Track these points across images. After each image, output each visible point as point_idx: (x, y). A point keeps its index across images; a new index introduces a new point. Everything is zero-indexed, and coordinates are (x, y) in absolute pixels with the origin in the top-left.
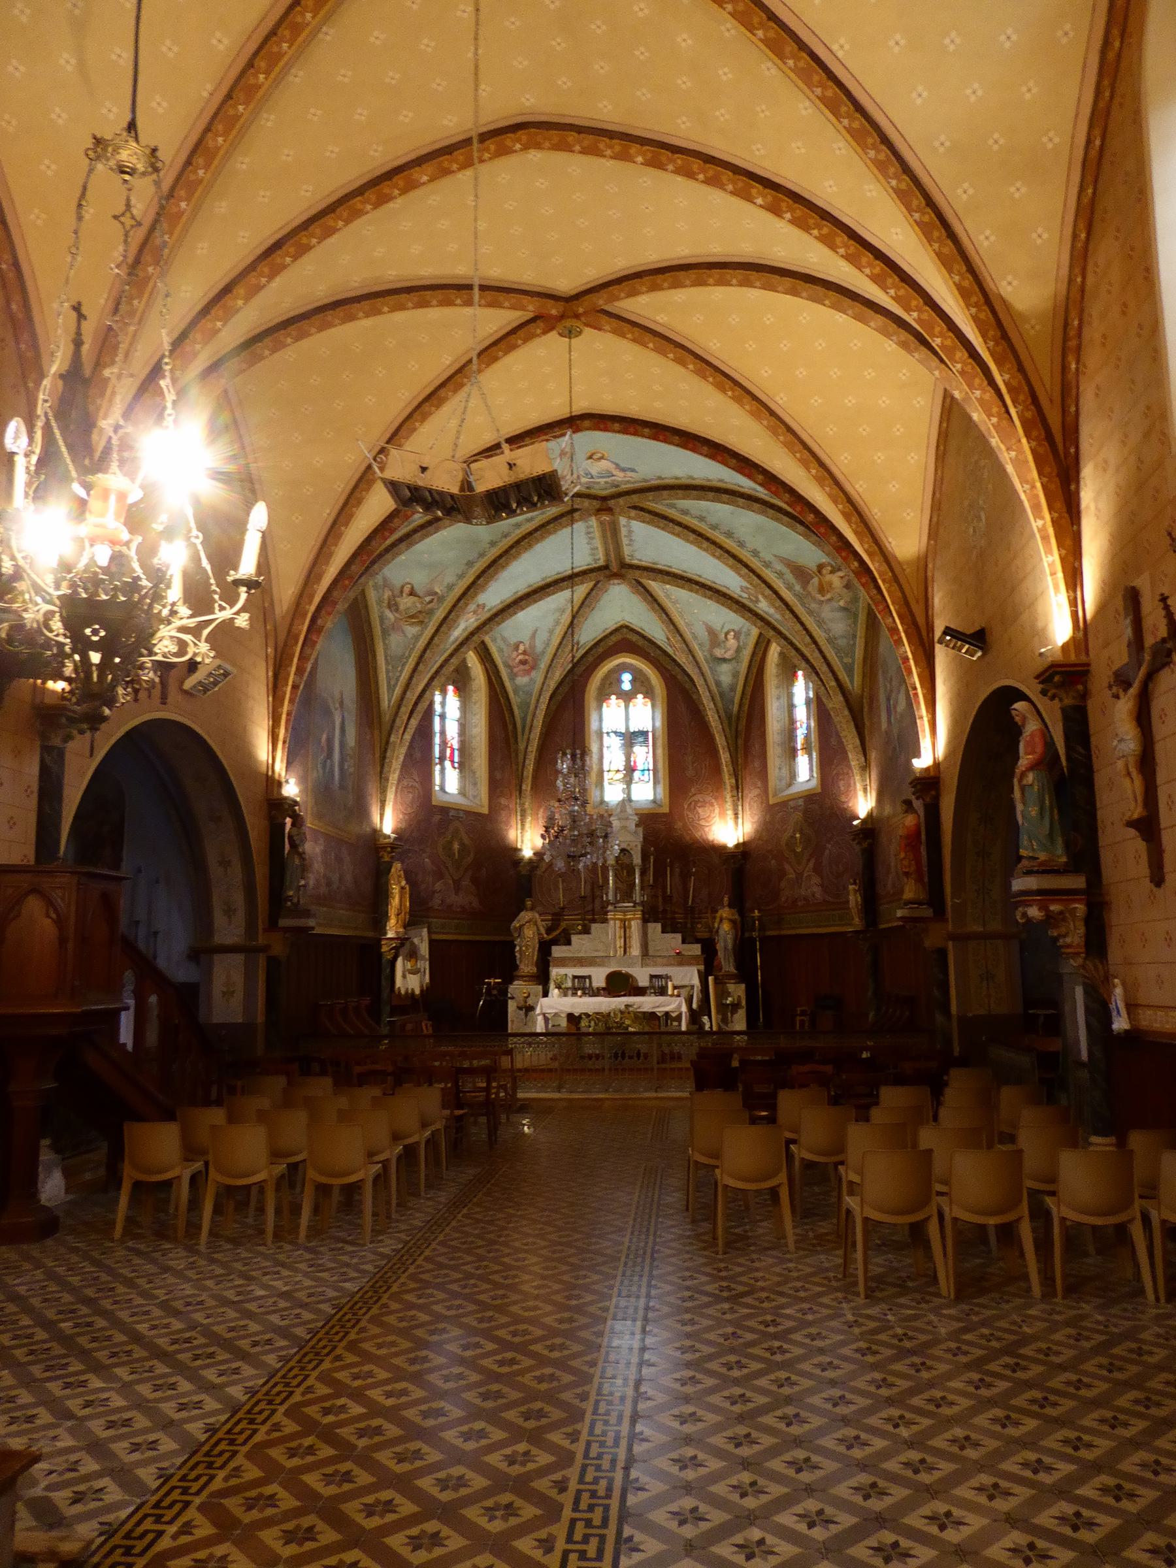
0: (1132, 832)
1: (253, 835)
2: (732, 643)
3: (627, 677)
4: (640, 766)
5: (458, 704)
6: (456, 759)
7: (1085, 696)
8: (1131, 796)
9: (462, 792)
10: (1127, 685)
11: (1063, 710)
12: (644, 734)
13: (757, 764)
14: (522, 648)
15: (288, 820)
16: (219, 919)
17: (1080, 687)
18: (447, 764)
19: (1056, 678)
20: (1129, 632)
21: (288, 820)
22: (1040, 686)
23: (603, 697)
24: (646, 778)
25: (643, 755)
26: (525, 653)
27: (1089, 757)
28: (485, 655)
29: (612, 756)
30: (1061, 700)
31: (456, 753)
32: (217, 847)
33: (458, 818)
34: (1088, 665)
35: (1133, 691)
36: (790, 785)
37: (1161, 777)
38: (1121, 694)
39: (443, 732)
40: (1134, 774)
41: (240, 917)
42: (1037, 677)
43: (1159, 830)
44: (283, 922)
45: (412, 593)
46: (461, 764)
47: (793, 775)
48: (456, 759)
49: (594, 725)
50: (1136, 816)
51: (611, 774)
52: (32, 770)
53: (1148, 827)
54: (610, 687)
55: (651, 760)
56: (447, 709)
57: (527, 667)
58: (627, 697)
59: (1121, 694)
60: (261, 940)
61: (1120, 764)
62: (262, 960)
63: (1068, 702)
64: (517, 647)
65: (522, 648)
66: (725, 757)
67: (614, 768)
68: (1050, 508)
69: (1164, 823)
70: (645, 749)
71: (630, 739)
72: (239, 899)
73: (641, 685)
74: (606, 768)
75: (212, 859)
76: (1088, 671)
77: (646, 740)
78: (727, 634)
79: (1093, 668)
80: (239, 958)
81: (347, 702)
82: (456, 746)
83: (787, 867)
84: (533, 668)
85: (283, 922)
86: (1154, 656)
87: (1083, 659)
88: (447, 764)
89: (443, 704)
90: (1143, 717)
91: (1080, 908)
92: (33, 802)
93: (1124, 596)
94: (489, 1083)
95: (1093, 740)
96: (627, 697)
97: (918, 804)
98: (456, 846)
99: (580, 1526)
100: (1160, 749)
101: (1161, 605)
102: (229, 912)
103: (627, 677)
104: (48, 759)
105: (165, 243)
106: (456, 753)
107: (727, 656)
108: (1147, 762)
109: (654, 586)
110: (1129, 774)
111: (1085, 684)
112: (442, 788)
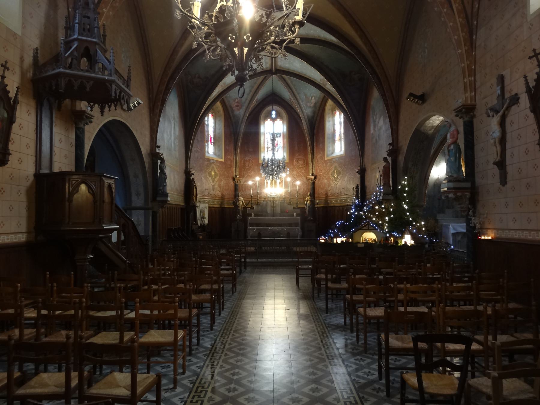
0: (496, 167)
1: (147, 166)
3: (274, 113)
5: (213, 121)
6: (212, 141)
7: (474, 116)
8: (495, 153)
9: (214, 154)
10: (497, 112)
11: (464, 122)
13: (321, 145)
14: (236, 101)
15: (159, 161)
16: (134, 198)
17: (472, 114)
18: (209, 143)
19: (464, 110)
20: (499, 92)
21: (159, 161)
22: (455, 114)
23: (265, 118)
25: (280, 141)
26: (238, 102)
27: (473, 140)
28: (223, 104)
30: (463, 119)
31: (212, 139)
32: (133, 170)
33: (213, 163)
34: (476, 105)
35: (500, 114)
36: (332, 153)
37: (508, 145)
38: (495, 115)
39: (208, 131)
40: (498, 145)
41: (142, 196)
42: (455, 110)
43: (506, 166)
44: (159, 199)
45: (199, 77)
46: (214, 143)
48: (212, 141)
50: (497, 160)
52: (73, 136)
53: (501, 164)
54: (269, 116)
56: (209, 123)
57: (238, 108)
58: (274, 120)
59: (495, 115)
60: (150, 205)
61: (492, 141)
62: (150, 212)
63: (466, 119)
64: (235, 101)
65: (236, 101)
66: (308, 142)
68: (465, 45)
69: (508, 163)
72: (142, 190)
73: (278, 115)
75: (131, 174)
76: (475, 108)
79: (477, 107)
80: (142, 212)
81: (175, 117)
82: (212, 137)
83: (331, 182)
84: (241, 108)
85: (159, 199)
86: (511, 100)
87: (473, 102)
88: (209, 143)
89: (208, 121)
90: (502, 124)
91: (468, 194)
92: (73, 149)
93: (497, 78)
95: (475, 134)
96: (274, 120)
97: (389, 159)
98: (213, 173)
99: (202, 396)
100: (508, 136)
101: (524, 79)
102: (138, 194)
103: (274, 113)
104: (78, 132)
106: (212, 139)
108: (503, 140)
109: (285, 77)
110: (495, 145)
111: (473, 113)
112: (208, 152)
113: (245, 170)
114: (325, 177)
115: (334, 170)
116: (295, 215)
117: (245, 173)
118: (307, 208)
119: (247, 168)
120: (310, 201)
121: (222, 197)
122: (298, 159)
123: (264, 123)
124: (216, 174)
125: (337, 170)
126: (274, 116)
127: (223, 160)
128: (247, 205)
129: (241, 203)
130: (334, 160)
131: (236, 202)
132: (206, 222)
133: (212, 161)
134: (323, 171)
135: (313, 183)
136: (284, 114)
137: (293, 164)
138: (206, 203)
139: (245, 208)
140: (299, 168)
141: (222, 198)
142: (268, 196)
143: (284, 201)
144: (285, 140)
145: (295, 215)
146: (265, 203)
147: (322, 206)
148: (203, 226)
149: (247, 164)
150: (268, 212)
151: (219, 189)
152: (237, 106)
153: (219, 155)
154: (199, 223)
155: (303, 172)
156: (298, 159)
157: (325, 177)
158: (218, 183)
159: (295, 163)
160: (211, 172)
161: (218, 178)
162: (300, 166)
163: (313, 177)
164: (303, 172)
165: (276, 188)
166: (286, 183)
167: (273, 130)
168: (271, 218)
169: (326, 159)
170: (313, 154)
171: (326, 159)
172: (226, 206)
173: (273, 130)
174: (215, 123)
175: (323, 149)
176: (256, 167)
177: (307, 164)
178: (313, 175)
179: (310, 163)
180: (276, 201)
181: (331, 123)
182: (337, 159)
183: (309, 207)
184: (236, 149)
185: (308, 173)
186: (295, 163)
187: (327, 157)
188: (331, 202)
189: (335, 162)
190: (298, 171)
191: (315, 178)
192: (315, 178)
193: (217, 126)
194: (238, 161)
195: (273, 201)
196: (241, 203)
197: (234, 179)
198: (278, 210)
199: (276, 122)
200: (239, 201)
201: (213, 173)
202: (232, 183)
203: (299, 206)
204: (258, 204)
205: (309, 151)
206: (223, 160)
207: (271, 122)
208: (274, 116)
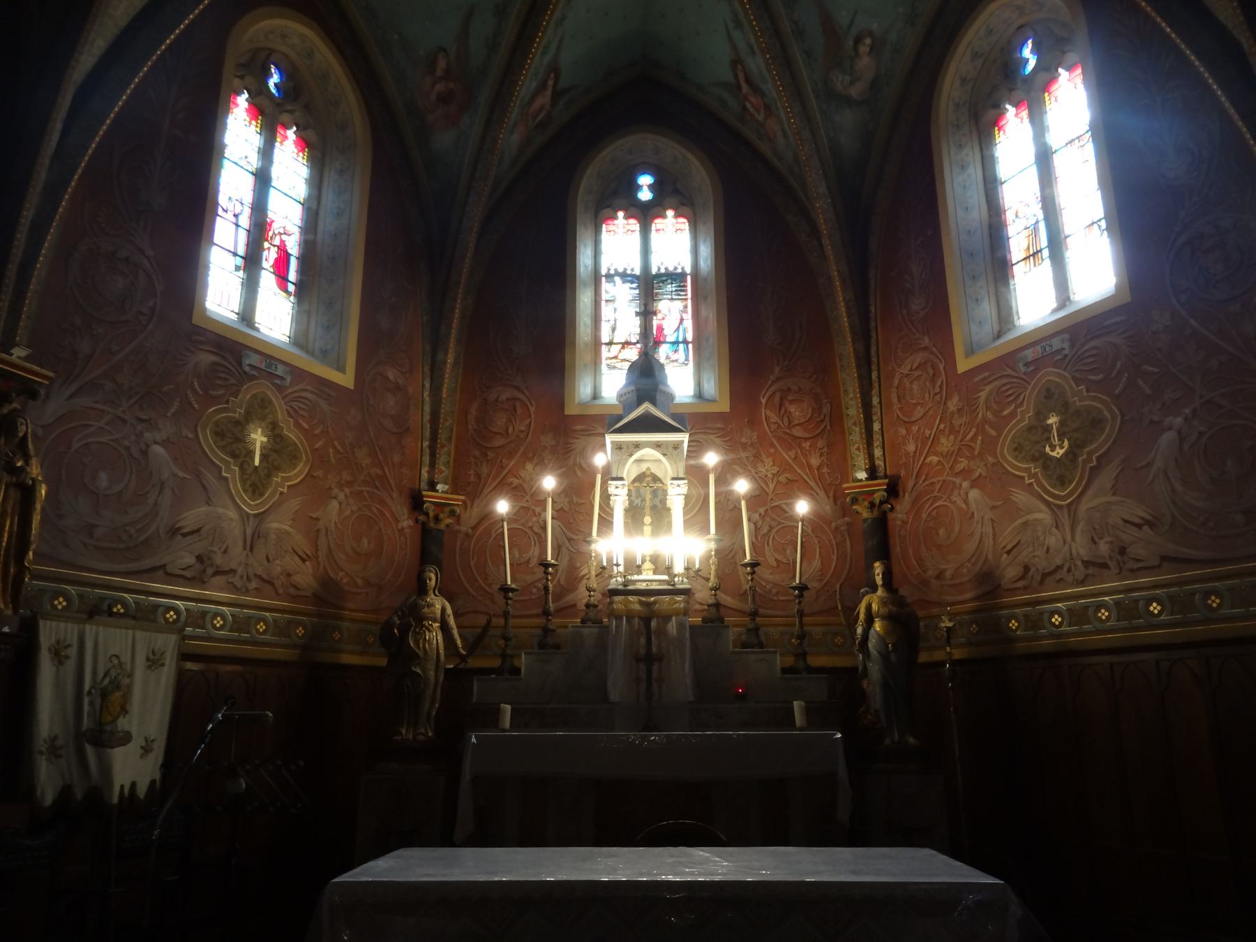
2: (865, 63)
4: (670, 336)
6: (292, 276)
9: (299, 339)
12: (676, 277)
13: (917, 304)
14: (442, 63)
23: (601, 211)
24: (681, 356)
25: (674, 315)
27: (453, 844)
29: (618, 314)
31: (293, 264)
36: (999, 336)
47: (1005, 316)
48: (292, 276)
49: (584, 259)
51: (615, 349)
54: (617, 196)
55: (689, 323)
67: (620, 337)
70: (679, 305)
71: (649, 286)
73: (673, 194)
74: (605, 338)
77: (682, 288)
78: (858, 40)
82: (293, 247)
94: (685, 420)
96: (646, 215)
98: (258, 438)
105: (493, 717)
106: (293, 264)
107: (855, 92)
113: (485, 455)
114: (965, 473)
115: (1041, 416)
116: (799, 719)
117: (485, 470)
118: (875, 670)
119: (499, 442)
120: (888, 617)
121: (318, 599)
122: (785, 392)
123: (597, 231)
124: (279, 450)
125: (1064, 409)
126: (645, 195)
127: (346, 379)
128: (475, 645)
129: (435, 636)
130: (1030, 354)
131: (405, 629)
132: (132, 768)
133: (251, 359)
134: (946, 444)
135: (881, 525)
136: (699, 174)
137: (753, 422)
138: (172, 627)
139: (458, 679)
140: (790, 442)
141: (327, 597)
142: (616, 582)
143: (715, 615)
144: (710, 313)
145: (799, 719)
146: (589, 631)
147: (958, 654)
148: (88, 809)
149: (500, 421)
150: (614, 696)
151: (300, 541)
152: (444, 99)
153: (325, 353)
154: (48, 780)
155: (815, 461)
156: (785, 392)
157: (965, 473)
158: (294, 504)
159: (768, 414)
160: (241, 425)
161: (298, 473)
162: (798, 432)
163: (880, 486)
164: (815, 461)
165: (656, 526)
166: (728, 508)
167: (641, 278)
168: (633, 735)
169: (963, 365)
170: (864, 362)
171: (963, 365)
172: (347, 659)
173: (641, 278)
174: (316, 182)
175: (938, 318)
176: (547, 440)
177: (837, 418)
178: (873, 473)
179: (853, 410)
180: (666, 618)
181: (975, 172)
182: (1056, 343)
183: (885, 656)
184: (436, 344)
185: (843, 469)
186: (768, 414)
187: (970, 352)
188: (1034, 623)
189: (1037, 364)
190: (787, 456)
191: (894, 490)
192: (894, 490)
193: (329, 196)
194: (445, 408)
195: (646, 620)
196: (435, 636)
197: (416, 502)
198: (680, 678)
199: (658, 223)
200: (420, 619)
201: (258, 438)
202: (406, 522)
203: (816, 661)
204: (546, 642)
205: (846, 349)
206: (346, 379)
207: (634, 225)
208: (645, 195)
